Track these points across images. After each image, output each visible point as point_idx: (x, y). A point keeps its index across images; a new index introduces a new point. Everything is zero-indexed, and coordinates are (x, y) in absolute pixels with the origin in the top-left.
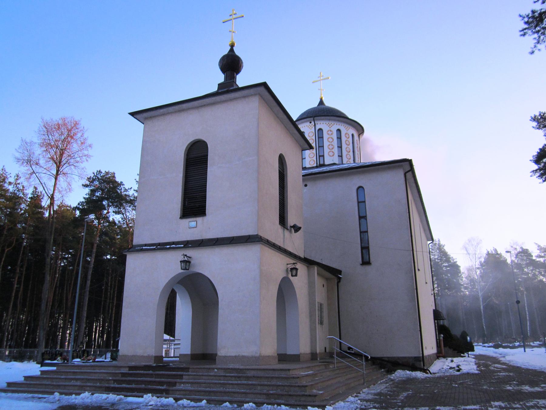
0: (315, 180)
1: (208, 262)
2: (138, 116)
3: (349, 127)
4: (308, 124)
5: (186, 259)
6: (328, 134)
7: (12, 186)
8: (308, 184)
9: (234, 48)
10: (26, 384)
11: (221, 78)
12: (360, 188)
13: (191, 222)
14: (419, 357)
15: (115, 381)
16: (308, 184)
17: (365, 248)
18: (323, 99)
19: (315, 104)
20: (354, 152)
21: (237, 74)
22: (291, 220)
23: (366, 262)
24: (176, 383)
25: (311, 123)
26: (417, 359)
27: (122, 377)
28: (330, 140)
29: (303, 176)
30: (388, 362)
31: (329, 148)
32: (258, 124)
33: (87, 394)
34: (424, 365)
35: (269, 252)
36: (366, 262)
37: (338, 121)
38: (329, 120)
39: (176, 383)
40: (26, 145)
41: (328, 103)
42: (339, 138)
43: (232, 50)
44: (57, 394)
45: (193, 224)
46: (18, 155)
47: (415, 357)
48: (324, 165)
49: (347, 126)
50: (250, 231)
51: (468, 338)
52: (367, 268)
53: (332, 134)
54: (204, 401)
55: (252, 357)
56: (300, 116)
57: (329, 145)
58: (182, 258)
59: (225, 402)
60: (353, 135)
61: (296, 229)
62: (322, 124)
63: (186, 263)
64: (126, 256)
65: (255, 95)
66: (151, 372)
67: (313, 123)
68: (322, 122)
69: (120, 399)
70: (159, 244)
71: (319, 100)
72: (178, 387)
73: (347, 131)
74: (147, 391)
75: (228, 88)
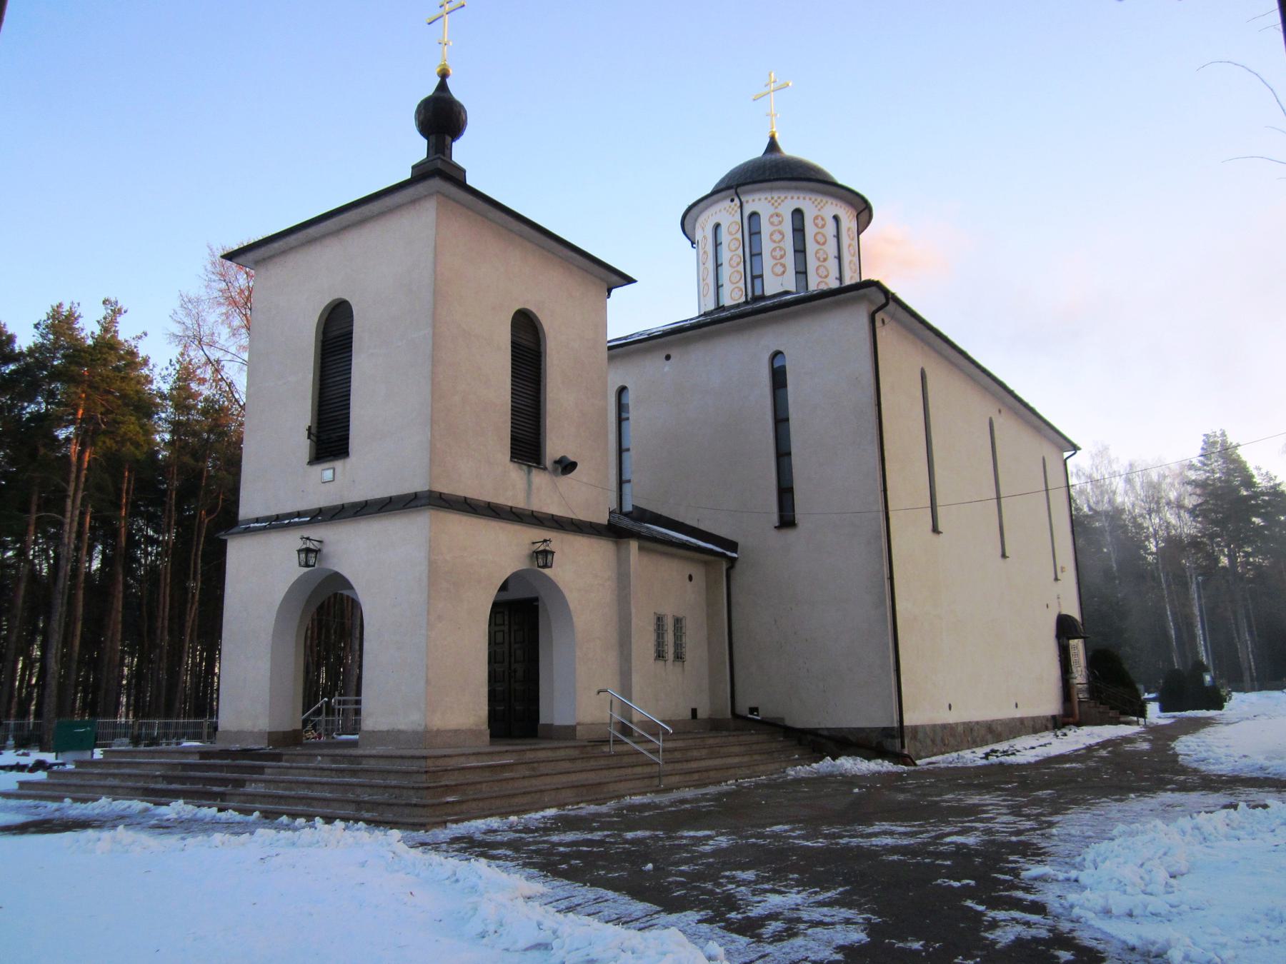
0: (688, 342)
1: (359, 553)
2: (241, 259)
3: (825, 199)
4: (727, 203)
5: (310, 545)
6: (772, 224)
7: (207, 385)
8: (673, 353)
9: (448, 81)
10: (54, 785)
11: (418, 149)
12: (777, 354)
13: (325, 471)
14: (892, 729)
15: (164, 777)
16: (673, 353)
17: (785, 492)
18: (777, 136)
19: (755, 150)
20: (839, 258)
21: (453, 140)
22: (554, 447)
23: (787, 521)
24: (245, 781)
25: (732, 200)
26: (887, 732)
27: (183, 770)
28: (777, 237)
29: (610, 348)
30: (829, 738)
31: (774, 258)
32: (436, 255)
33: (104, 801)
34: (903, 746)
35: (459, 526)
36: (787, 521)
37: (796, 189)
38: (772, 189)
39: (245, 781)
40: (189, 303)
41: (791, 149)
42: (799, 230)
43: (442, 87)
44: (68, 801)
45: (328, 474)
46: (178, 330)
47: (884, 729)
48: (763, 298)
49: (819, 198)
50: (415, 483)
51: (1208, 678)
52: (790, 535)
53: (780, 223)
54: (257, 814)
55: (415, 733)
56: (722, 181)
57: (774, 250)
58: (300, 545)
59: (281, 814)
60: (836, 218)
61: (566, 466)
62: (759, 202)
63: (310, 554)
64: (225, 541)
65: (430, 195)
66: (228, 762)
67: (737, 201)
68: (756, 196)
69: (147, 810)
70: (278, 518)
71: (768, 140)
72: (250, 788)
73: (819, 210)
74: (176, 795)
75: (438, 172)
